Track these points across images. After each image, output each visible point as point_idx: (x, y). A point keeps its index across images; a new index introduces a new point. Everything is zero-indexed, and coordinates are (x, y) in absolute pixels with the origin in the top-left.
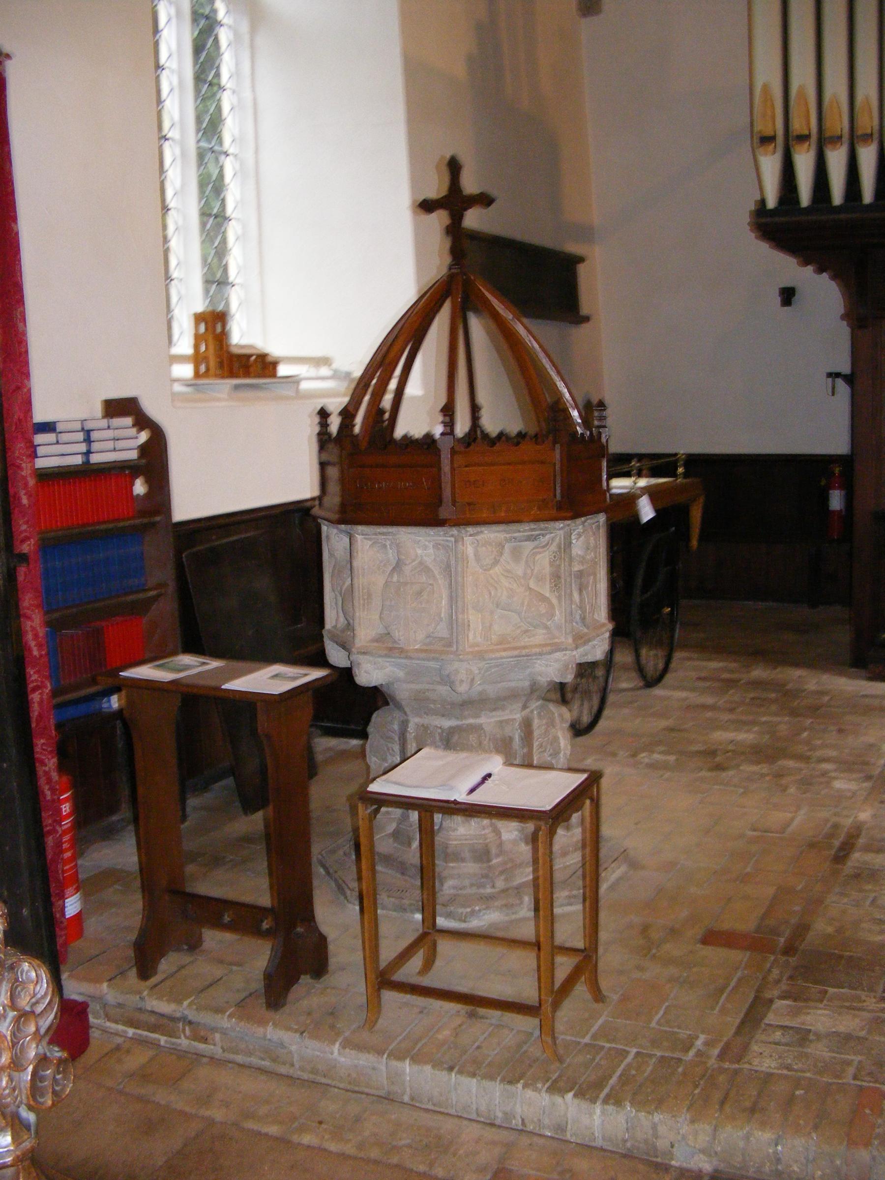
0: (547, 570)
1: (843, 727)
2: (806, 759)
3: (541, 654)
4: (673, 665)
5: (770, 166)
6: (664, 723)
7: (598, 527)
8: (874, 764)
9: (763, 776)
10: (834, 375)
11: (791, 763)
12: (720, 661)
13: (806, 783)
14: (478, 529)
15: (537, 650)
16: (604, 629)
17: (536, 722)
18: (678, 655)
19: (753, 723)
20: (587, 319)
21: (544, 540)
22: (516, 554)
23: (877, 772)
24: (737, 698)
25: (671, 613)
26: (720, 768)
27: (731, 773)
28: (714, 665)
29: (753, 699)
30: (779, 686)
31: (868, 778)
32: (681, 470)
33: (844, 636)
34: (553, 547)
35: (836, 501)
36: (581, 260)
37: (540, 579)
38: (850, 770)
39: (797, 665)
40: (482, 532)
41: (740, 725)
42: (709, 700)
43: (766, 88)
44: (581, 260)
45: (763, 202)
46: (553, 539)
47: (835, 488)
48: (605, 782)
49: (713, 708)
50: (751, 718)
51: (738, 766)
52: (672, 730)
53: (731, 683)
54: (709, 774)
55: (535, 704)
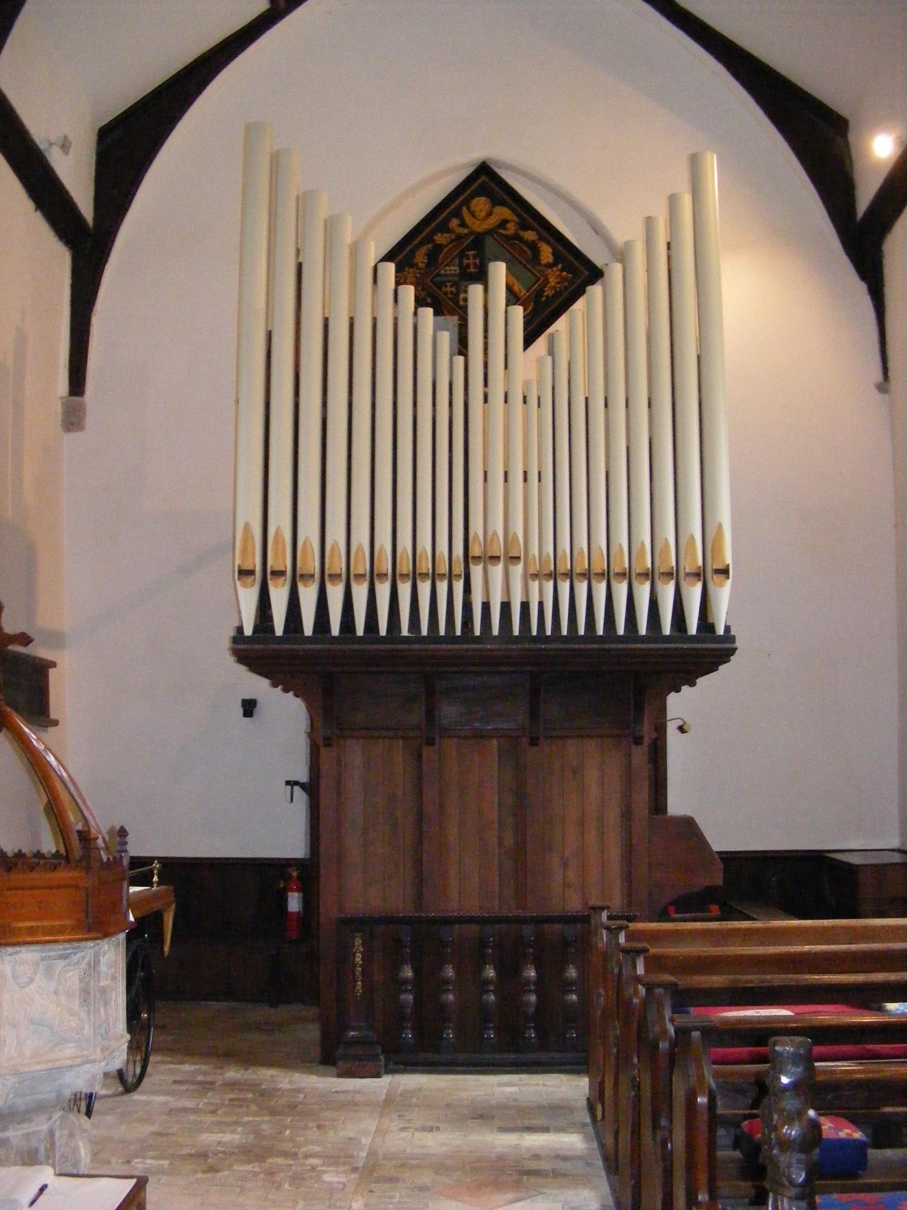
0: (77, 986)
1: (322, 1123)
2: (294, 1156)
3: (71, 1066)
4: (149, 1069)
5: (248, 598)
6: (152, 1129)
7: (118, 944)
8: (357, 1157)
9: (256, 1174)
10: (291, 783)
11: (280, 1161)
12: (193, 1064)
13: (297, 1179)
14: (17, 949)
15: (69, 1062)
16: (123, 1040)
17: (57, 1134)
18: (152, 1058)
19: (237, 1123)
20: (55, 723)
21: (75, 958)
22: (49, 971)
23: (361, 1165)
24: (216, 1100)
25: (149, 1019)
26: (213, 1169)
27: (226, 1173)
28: (187, 1067)
29: (231, 1100)
30: (253, 1086)
31: (355, 1169)
32: (155, 879)
33: (312, 1033)
34: (84, 965)
35: (294, 903)
36: (53, 665)
37: (69, 994)
38: (336, 1164)
39: (269, 1064)
40: (20, 952)
41: (222, 1126)
42: (190, 1104)
43: (247, 527)
44: (53, 665)
45: (240, 629)
46: (83, 957)
47: (293, 890)
48: (149, 1188)
49: (195, 1111)
50: (234, 1119)
51: (231, 1166)
52: (160, 1134)
53: (208, 1086)
54: (205, 1176)
55: (58, 1115)
